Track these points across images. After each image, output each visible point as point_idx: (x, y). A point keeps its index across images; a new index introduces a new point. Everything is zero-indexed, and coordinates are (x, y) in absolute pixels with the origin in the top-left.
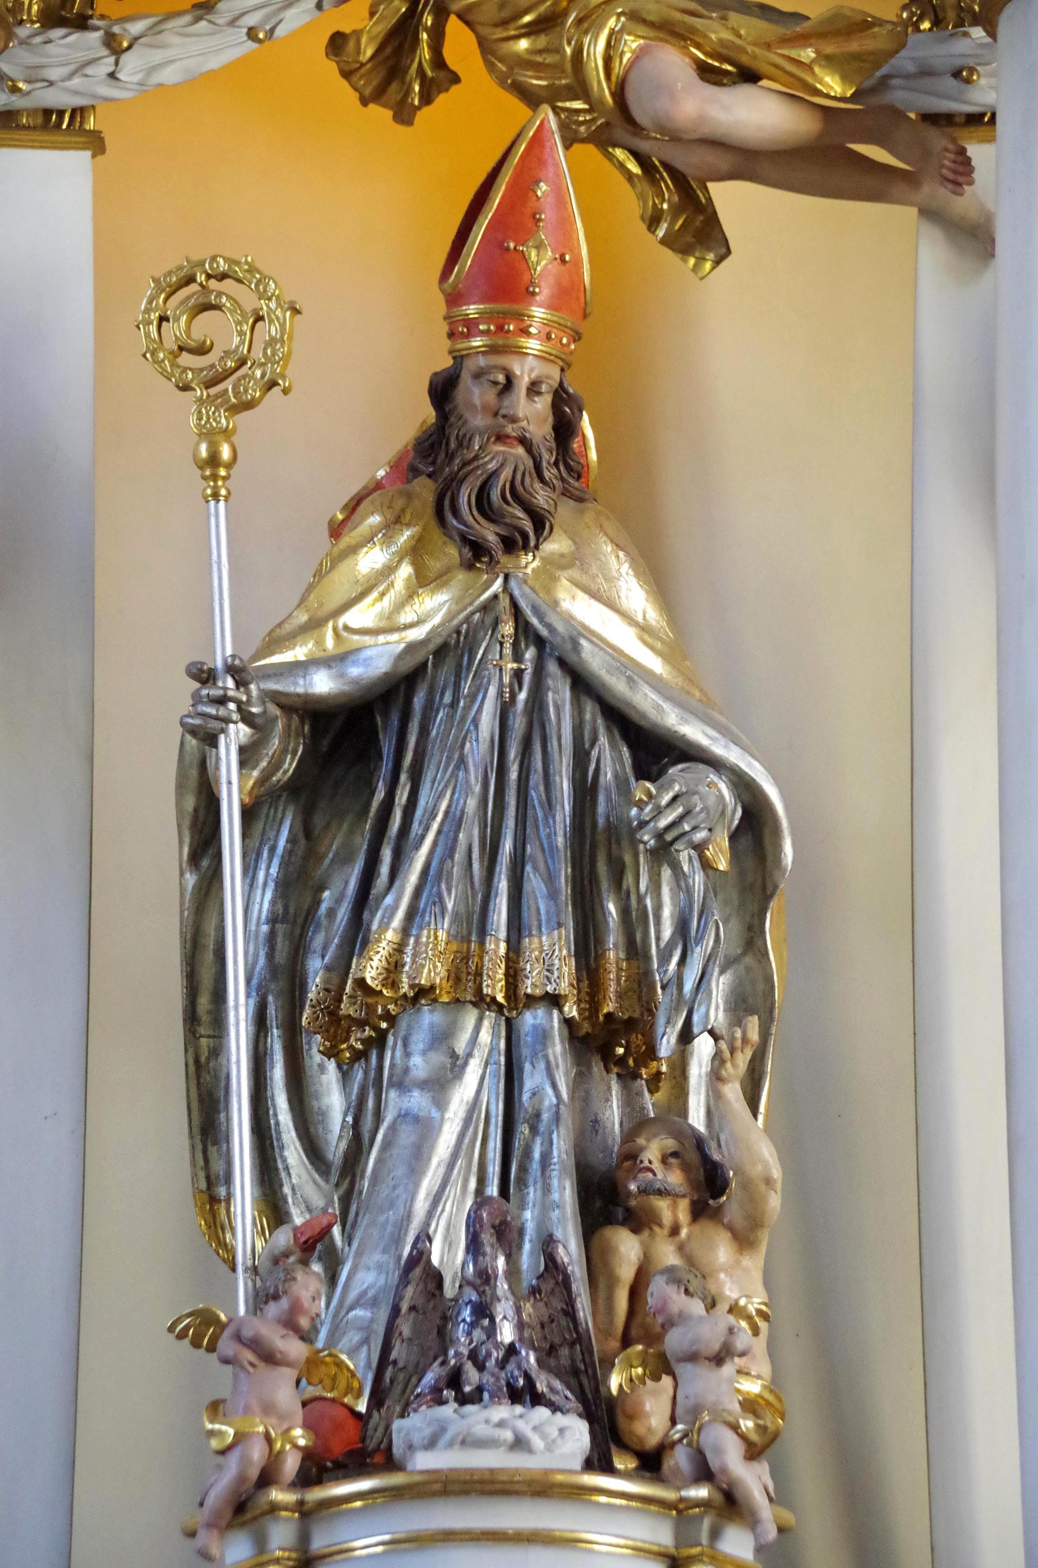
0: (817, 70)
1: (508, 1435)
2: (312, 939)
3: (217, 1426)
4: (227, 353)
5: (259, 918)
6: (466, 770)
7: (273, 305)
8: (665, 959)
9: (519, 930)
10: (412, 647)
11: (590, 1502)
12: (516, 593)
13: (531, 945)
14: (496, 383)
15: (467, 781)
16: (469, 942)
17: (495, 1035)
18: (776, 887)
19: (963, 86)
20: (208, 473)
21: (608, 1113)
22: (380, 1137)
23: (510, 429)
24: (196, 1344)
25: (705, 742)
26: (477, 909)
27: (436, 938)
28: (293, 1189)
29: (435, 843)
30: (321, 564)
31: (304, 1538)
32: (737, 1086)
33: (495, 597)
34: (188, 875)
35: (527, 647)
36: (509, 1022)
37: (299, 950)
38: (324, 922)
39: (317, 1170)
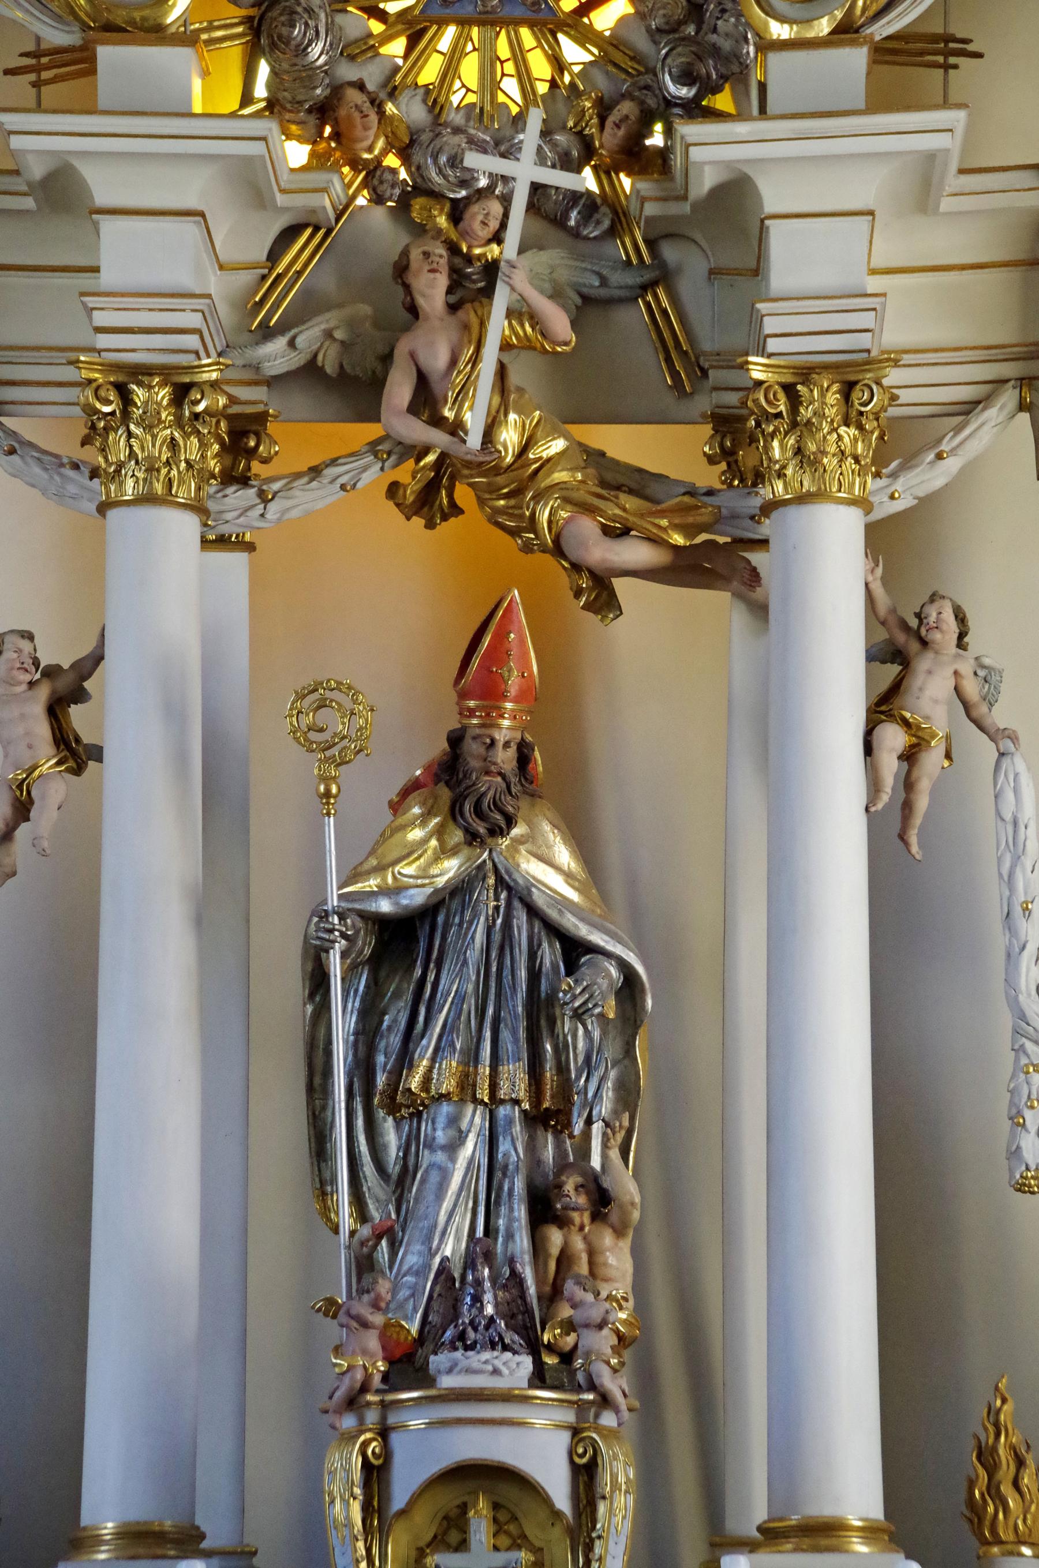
0: (670, 532)
1: (490, 1368)
2: (378, 1043)
3: (338, 1361)
4: (335, 734)
5: (348, 1032)
6: (468, 968)
7: (361, 708)
8: (578, 1078)
9: (497, 1062)
10: (437, 891)
11: (532, 1403)
12: (496, 860)
13: (505, 1070)
14: (485, 743)
15: (469, 975)
16: (469, 1066)
17: (483, 1119)
18: (642, 1021)
19: (756, 524)
20: (324, 801)
21: (546, 1154)
22: (419, 1176)
23: (493, 768)
24: (326, 1314)
25: (602, 944)
26: (473, 1047)
27: (451, 1065)
28: (369, 1189)
29: (450, 1009)
30: (385, 831)
31: (384, 1418)
32: (617, 1150)
33: (485, 861)
34: (308, 1006)
35: (502, 891)
36: (491, 1112)
37: (371, 1049)
38: (385, 1033)
39: (383, 1179)
